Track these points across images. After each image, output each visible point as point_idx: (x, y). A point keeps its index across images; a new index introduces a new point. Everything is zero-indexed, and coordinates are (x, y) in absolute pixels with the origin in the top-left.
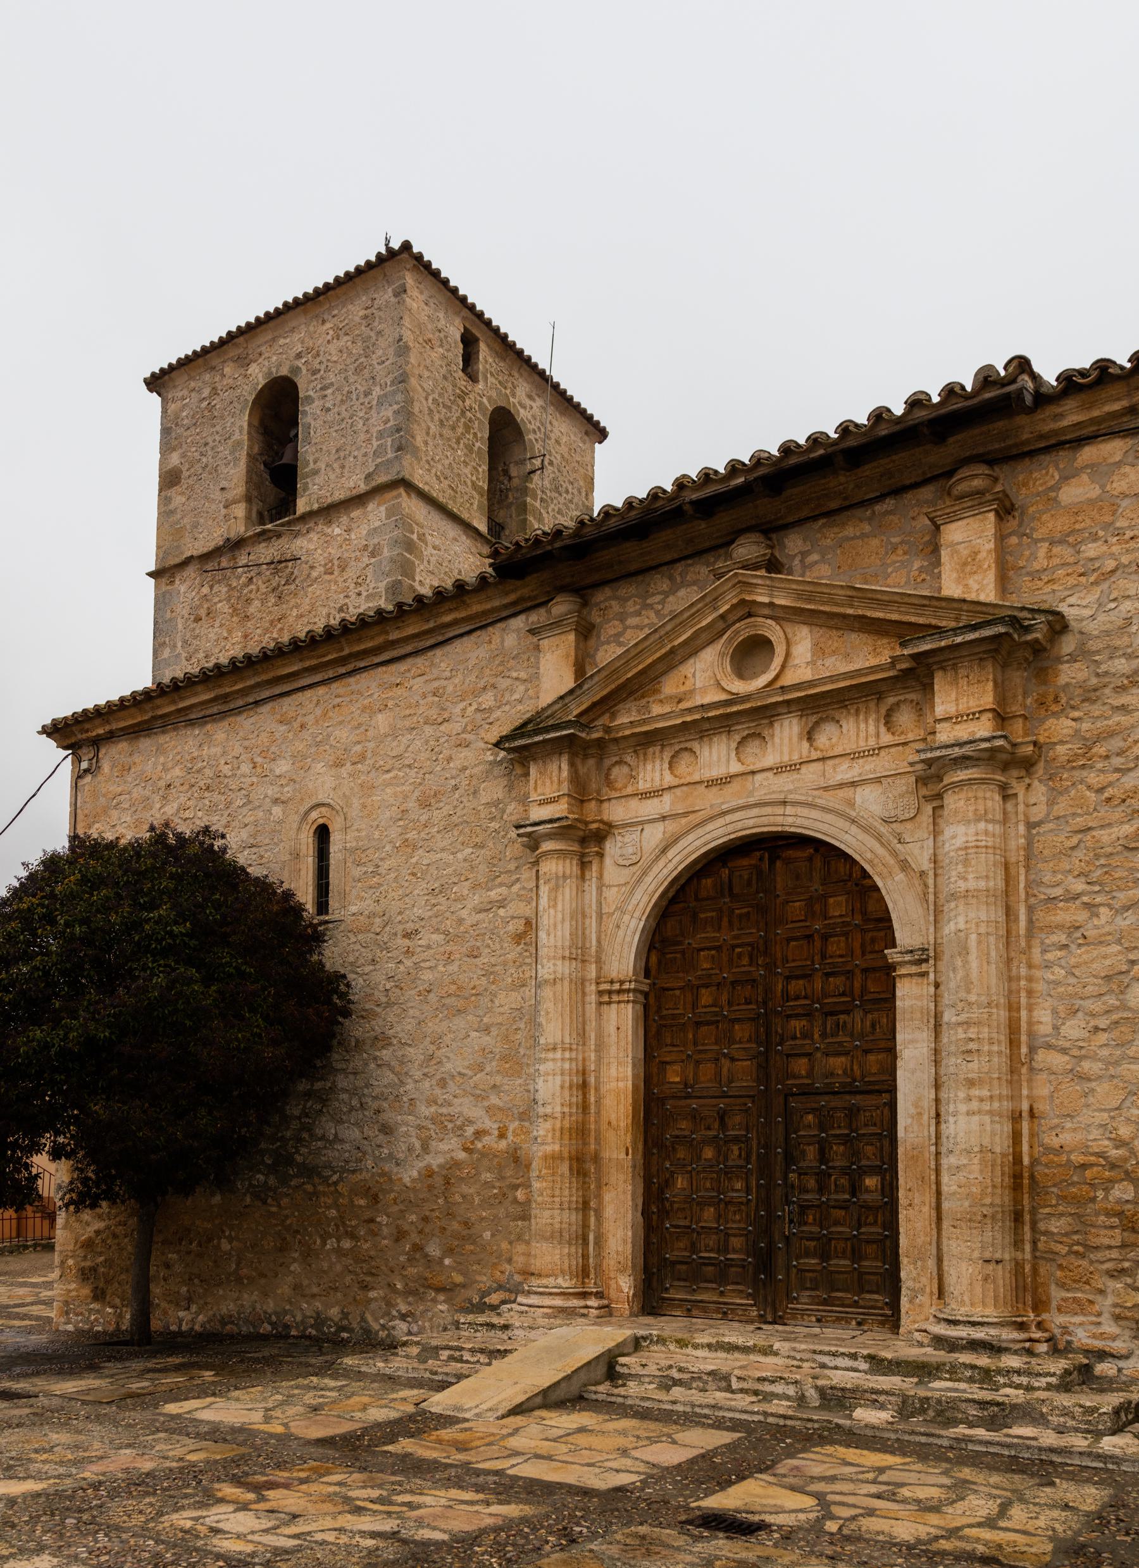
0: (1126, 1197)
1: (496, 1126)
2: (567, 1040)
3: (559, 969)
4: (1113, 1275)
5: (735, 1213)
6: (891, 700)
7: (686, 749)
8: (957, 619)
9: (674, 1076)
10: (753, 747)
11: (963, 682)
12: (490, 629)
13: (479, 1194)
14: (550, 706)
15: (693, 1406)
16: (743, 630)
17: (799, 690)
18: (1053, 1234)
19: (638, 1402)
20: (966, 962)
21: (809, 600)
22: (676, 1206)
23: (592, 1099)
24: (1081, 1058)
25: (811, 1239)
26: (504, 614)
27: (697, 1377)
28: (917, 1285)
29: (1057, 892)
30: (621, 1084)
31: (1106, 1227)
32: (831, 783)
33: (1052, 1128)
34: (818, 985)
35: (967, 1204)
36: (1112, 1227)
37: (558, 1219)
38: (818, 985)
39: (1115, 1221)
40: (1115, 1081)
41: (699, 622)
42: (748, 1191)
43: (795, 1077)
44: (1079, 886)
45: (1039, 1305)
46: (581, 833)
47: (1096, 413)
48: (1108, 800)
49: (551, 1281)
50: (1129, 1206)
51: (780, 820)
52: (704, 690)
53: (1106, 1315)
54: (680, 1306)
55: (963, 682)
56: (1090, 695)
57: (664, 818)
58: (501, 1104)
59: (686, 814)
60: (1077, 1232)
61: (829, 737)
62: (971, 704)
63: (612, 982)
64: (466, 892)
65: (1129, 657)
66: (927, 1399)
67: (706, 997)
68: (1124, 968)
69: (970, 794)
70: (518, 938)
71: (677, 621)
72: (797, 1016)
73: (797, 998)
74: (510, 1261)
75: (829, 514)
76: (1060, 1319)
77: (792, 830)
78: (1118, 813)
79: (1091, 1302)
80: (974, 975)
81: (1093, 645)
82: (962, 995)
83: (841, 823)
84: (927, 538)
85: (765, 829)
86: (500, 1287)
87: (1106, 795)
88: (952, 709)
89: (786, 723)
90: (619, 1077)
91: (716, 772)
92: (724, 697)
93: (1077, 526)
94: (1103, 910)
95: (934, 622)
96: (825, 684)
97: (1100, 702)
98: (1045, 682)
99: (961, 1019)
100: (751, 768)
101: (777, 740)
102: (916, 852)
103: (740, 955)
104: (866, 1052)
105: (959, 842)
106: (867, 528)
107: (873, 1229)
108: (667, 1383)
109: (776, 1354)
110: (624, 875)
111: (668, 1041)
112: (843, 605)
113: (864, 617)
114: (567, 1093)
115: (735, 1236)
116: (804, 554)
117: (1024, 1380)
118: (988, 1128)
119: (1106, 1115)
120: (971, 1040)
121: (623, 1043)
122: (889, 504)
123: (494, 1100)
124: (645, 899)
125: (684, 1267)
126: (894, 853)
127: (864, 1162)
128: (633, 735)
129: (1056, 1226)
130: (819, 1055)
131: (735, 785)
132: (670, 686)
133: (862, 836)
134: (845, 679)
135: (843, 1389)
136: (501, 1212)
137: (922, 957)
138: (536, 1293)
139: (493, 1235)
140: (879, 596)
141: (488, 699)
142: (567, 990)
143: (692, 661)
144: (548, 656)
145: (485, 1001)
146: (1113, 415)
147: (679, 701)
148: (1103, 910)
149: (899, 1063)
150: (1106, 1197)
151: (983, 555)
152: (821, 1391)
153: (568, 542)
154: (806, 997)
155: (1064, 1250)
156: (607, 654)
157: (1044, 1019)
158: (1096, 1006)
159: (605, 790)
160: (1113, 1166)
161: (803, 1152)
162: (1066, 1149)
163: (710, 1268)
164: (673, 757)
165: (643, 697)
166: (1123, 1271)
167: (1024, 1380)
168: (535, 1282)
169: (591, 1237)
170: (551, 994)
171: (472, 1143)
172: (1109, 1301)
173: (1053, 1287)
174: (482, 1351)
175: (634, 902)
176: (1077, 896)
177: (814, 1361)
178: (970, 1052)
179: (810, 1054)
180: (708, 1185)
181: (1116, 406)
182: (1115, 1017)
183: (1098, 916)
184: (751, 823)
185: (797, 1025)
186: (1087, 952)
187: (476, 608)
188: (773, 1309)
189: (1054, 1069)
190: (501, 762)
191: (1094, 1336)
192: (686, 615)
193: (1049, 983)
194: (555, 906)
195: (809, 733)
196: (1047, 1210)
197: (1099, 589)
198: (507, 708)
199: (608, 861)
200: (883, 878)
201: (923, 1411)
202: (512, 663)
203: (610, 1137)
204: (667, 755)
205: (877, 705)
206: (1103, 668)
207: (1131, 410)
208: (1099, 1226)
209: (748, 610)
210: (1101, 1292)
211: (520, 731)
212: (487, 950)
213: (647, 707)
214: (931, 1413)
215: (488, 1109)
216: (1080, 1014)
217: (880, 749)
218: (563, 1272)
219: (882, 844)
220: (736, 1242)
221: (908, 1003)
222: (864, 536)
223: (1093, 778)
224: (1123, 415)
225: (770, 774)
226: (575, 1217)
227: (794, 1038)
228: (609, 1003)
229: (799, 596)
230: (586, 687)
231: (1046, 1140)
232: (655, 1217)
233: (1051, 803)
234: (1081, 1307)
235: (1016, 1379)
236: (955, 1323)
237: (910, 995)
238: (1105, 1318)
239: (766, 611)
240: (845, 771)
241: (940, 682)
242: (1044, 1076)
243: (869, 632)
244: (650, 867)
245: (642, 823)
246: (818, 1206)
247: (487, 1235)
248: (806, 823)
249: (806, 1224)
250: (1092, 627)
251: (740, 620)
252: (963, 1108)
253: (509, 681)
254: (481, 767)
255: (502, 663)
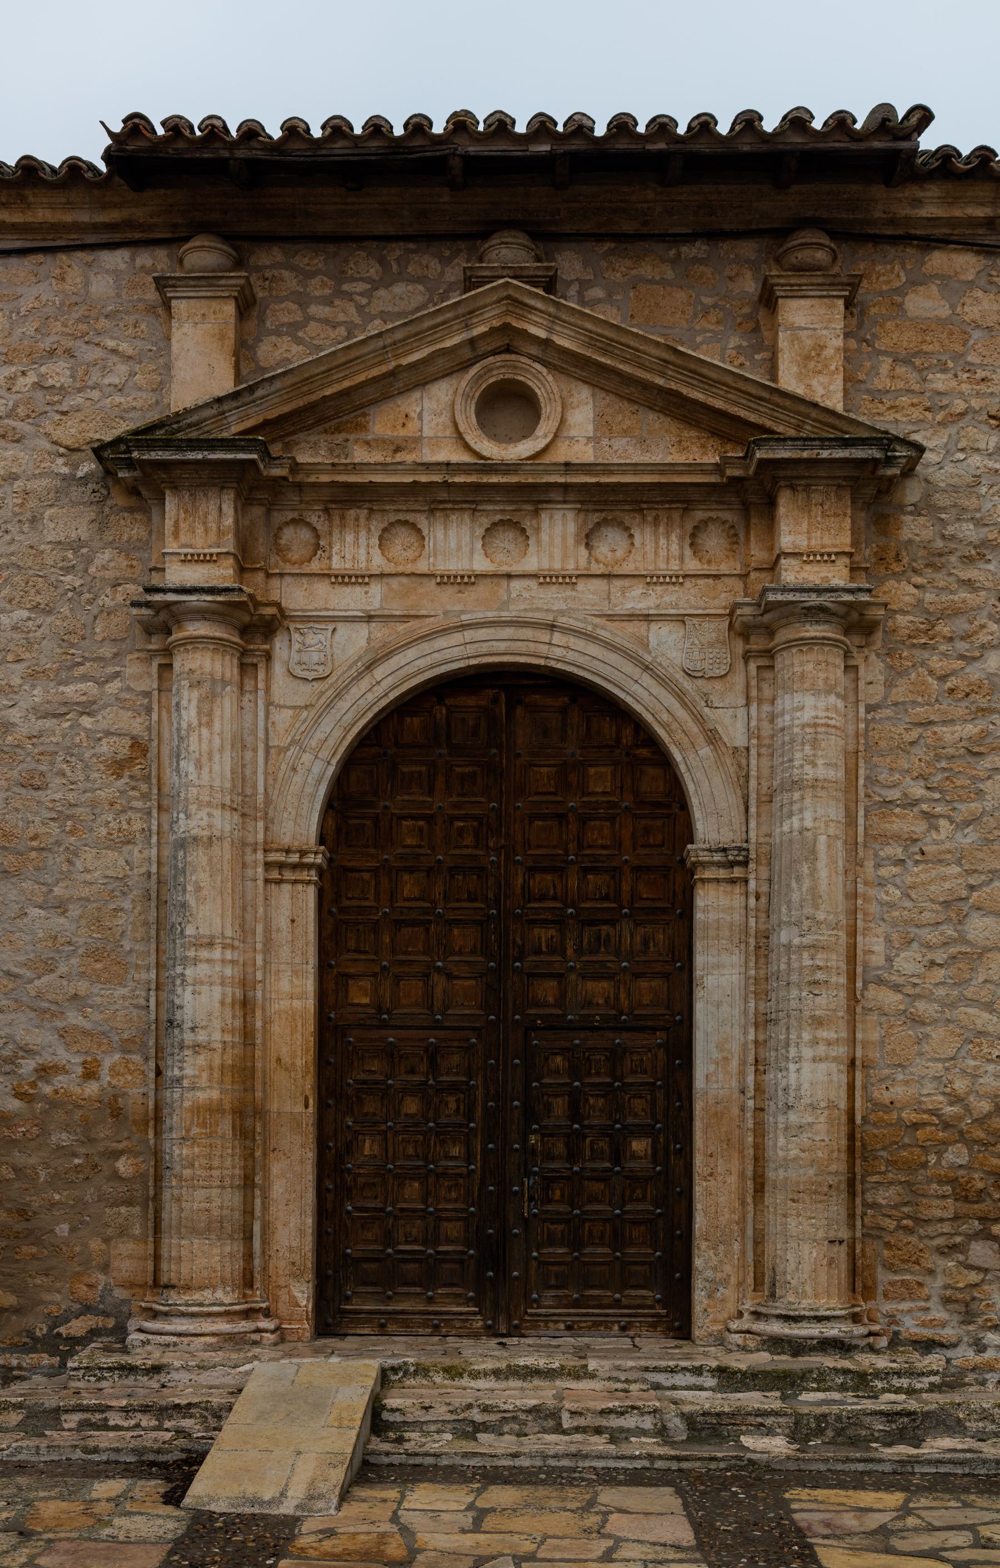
0: (960, 1161)
1: (78, 1059)
2: (229, 933)
3: (217, 822)
4: (943, 1252)
5: (449, 1189)
6: (700, 515)
7: (406, 523)
8: (798, 428)
9: (360, 996)
10: (505, 539)
11: (817, 511)
12: (63, 257)
13: (46, 1165)
14: (198, 408)
15: (545, 1457)
16: (498, 369)
17: (589, 473)
18: (880, 1206)
19: (458, 1460)
20: (813, 871)
21: (605, 352)
22: (361, 1180)
23: (259, 1024)
24: (914, 997)
25: (559, 1222)
26: (91, 239)
27: (509, 1417)
28: (719, 1275)
29: (894, 794)
30: (297, 1004)
31: (938, 1197)
32: (618, 610)
33: (881, 1080)
34: (573, 882)
35: (811, 1172)
36: (944, 1197)
37: (217, 1202)
38: (573, 882)
39: (948, 1189)
40: (951, 1026)
41: (442, 339)
42: (469, 1158)
43: (537, 1004)
44: (918, 791)
45: (868, 1292)
46: (247, 619)
47: (957, 213)
48: (951, 691)
49: (207, 1296)
50: (962, 1172)
51: (543, 649)
52: (436, 442)
53: (935, 1299)
54: (369, 1321)
55: (817, 511)
56: (935, 561)
57: (369, 618)
58: (88, 1026)
59: (405, 618)
60: (906, 1204)
61: (611, 545)
62: (827, 541)
63: (288, 851)
64: (16, 681)
65: (979, 523)
66: (825, 1416)
67: (409, 886)
68: (964, 893)
69: (820, 658)
70: (118, 767)
71: (412, 329)
72: (543, 923)
73: (543, 898)
74: (105, 1268)
75: (620, 237)
76: (887, 1307)
77: (560, 666)
78: (960, 710)
79: (920, 1285)
80: (823, 886)
81: (941, 500)
82: (808, 910)
83: (628, 667)
84: (747, 310)
85: (522, 660)
86: (87, 1309)
87: (949, 684)
88: (802, 543)
89: (558, 515)
90: (292, 991)
91: (454, 565)
92: (466, 458)
93: (925, 348)
94: (943, 822)
95: (769, 424)
96: (624, 473)
97: (944, 571)
98: (885, 533)
99: (807, 940)
100: (505, 569)
101: (544, 537)
102: (727, 721)
103: (461, 831)
104: (637, 976)
105: (807, 716)
106: (670, 274)
107: (641, 1207)
108: (469, 1430)
109: (593, 1376)
110: (303, 694)
111: (352, 944)
112: (650, 370)
113: (678, 394)
114: (228, 1013)
115: (449, 1220)
116: (584, 285)
117: (905, 1382)
118: (835, 1079)
119: (940, 1065)
120: (819, 968)
121: (300, 944)
122: (698, 249)
123: (74, 1018)
124: (337, 733)
125: (373, 1266)
126: (699, 719)
127: (630, 1120)
128: (333, 484)
129: (884, 1196)
130: (573, 977)
131: (482, 590)
132: (382, 423)
133: (657, 689)
134: (652, 472)
135: (718, 1415)
136: (90, 1194)
137: (737, 860)
138: (183, 1315)
139: (73, 1230)
140: (705, 371)
141: (58, 373)
142: (228, 856)
143: (417, 394)
144: (187, 328)
145: (56, 861)
146: (972, 222)
147: (397, 450)
148: (943, 822)
149: (698, 993)
150: (938, 1162)
151: (829, 352)
152: (689, 1419)
153: (259, 154)
154: (554, 898)
155: (892, 1225)
156: (279, 352)
157: (875, 948)
158: (931, 936)
159: (274, 559)
160: (946, 1126)
161: (549, 1108)
162: (898, 1105)
163: (412, 1266)
164: (385, 530)
165: (338, 430)
166: (954, 1248)
167: (905, 1382)
168: (174, 1297)
169: (257, 1228)
170: (204, 860)
171: (33, 1085)
172: (940, 1281)
173: (880, 1269)
174: (145, 1409)
175: (320, 735)
176: (916, 802)
177: (645, 1381)
178: (816, 983)
179: (560, 976)
180: (410, 1150)
181: (980, 212)
182: (953, 950)
183: (937, 829)
184: (502, 646)
185: (543, 935)
186: (926, 871)
187: (43, 215)
188: (504, 1314)
189: (886, 1009)
190: (85, 480)
191: (923, 1325)
192: (427, 324)
193: (882, 904)
194: (209, 725)
195: (587, 536)
196: (875, 1178)
197: (947, 432)
198: (95, 394)
199: (278, 668)
200: (682, 750)
201: (820, 1432)
202: (103, 323)
203: (280, 1079)
204: (486, 522)
205: (682, 517)
206: (950, 530)
207: (989, 223)
208: (932, 1196)
209: (508, 340)
210: (931, 1272)
211: (144, 436)
212: (59, 780)
213: (344, 447)
214: (830, 1433)
215: (63, 1034)
216: (915, 945)
217: (685, 576)
218: (224, 1281)
219: (684, 704)
220: (452, 1229)
221: (712, 916)
222: (663, 282)
223: (936, 663)
224: (981, 225)
225: (533, 583)
226: (234, 1199)
227: (538, 952)
228: (279, 882)
229: (592, 340)
230: (259, 393)
231: (876, 1094)
232: (330, 1197)
233: (889, 684)
234: (910, 1291)
235: (896, 1382)
236: (797, 1319)
237: (713, 905)
238: (934, 1303)
239: (534, 350)
240: (637, 599)
241: (785, 505)
242: (874, 1017)
243: (674, 417)
244: (347, 688)
245: (334, 619)
246: (568, 1178)
247: (63, 1229)
248: (581, 660)
249: (550, 1201)
250: (939, 477)
251: (494, 353)
252: (808, 1053)
253: (98, 353)
254: (45, 482)
255: (84, 319)
